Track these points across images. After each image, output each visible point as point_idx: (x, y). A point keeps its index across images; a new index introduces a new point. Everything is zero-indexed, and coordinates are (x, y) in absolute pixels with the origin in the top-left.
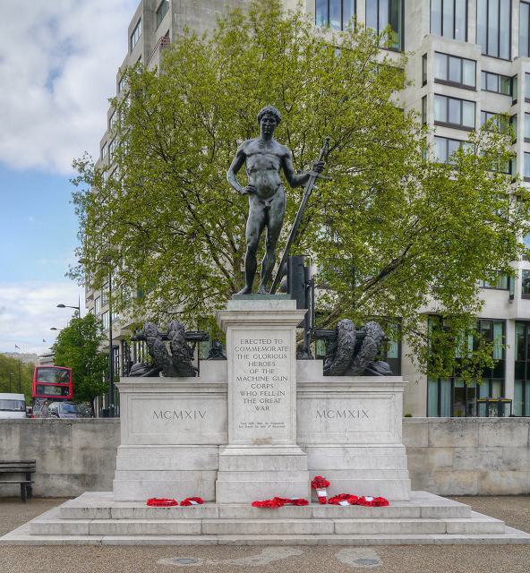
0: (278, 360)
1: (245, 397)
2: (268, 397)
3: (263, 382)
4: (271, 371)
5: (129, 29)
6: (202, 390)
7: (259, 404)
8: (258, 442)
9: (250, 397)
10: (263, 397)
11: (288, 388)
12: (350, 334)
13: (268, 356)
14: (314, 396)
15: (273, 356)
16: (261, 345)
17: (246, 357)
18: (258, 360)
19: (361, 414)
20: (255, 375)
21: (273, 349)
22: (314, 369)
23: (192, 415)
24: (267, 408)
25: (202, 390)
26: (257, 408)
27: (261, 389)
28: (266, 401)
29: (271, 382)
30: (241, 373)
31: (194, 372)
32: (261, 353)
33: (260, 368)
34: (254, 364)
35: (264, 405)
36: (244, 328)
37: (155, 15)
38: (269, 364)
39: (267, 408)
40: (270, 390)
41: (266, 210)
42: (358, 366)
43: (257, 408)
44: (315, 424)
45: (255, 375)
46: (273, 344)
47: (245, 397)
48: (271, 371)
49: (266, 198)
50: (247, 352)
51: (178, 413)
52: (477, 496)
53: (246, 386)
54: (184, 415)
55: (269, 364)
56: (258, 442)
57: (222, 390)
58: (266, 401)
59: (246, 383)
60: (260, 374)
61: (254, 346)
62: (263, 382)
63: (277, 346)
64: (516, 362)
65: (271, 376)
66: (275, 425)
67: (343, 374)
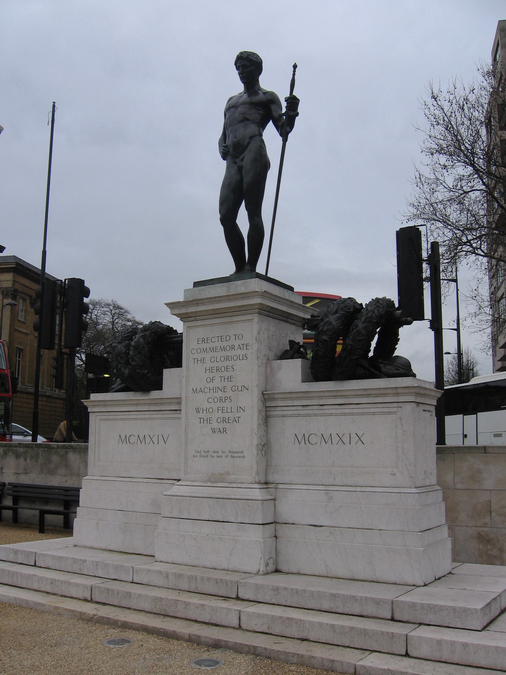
0: (238, 362)
1: (201, 415)
2: (226, 415)
3: (220, 394)
4: (230, 379)
7: (215, 425)
8: (215, 479)
10: (220, 414)
11: (251, 401)
13: (227, 358)
14: (290, 413)
15: (232, 358)
16: (219, 344)
17: (203, 360)
18: (215, 365)
20: (211, 385)
21: (233, 348)
22: (291, 373)
23: (155, 440)
24: (225, 430)
27: (219, 404)
28: (224, 420)
29: (229, 393)
33: (217, 375)
34: (211, 370)
35: (221, 426)
36: (200, 323)
38: (227, 369)
39: (225, 430)
40: (227, 404)
41: (240, 169)
43: (214, 432)
44: (290, 458)
45: (211, 385)
46: (232, 342)
47: (201, 415)
48: (230, 379)
49: (237, 157)
50: (203, 355)
52: (420, 624)
54: (148, 440)
56: (215, 479)
57: (176, 406)
58: (224, 420)
60: (217, 383)
62: (220, 394)
63: (237, 343)
64: (240, 78)
65: (229, 385)
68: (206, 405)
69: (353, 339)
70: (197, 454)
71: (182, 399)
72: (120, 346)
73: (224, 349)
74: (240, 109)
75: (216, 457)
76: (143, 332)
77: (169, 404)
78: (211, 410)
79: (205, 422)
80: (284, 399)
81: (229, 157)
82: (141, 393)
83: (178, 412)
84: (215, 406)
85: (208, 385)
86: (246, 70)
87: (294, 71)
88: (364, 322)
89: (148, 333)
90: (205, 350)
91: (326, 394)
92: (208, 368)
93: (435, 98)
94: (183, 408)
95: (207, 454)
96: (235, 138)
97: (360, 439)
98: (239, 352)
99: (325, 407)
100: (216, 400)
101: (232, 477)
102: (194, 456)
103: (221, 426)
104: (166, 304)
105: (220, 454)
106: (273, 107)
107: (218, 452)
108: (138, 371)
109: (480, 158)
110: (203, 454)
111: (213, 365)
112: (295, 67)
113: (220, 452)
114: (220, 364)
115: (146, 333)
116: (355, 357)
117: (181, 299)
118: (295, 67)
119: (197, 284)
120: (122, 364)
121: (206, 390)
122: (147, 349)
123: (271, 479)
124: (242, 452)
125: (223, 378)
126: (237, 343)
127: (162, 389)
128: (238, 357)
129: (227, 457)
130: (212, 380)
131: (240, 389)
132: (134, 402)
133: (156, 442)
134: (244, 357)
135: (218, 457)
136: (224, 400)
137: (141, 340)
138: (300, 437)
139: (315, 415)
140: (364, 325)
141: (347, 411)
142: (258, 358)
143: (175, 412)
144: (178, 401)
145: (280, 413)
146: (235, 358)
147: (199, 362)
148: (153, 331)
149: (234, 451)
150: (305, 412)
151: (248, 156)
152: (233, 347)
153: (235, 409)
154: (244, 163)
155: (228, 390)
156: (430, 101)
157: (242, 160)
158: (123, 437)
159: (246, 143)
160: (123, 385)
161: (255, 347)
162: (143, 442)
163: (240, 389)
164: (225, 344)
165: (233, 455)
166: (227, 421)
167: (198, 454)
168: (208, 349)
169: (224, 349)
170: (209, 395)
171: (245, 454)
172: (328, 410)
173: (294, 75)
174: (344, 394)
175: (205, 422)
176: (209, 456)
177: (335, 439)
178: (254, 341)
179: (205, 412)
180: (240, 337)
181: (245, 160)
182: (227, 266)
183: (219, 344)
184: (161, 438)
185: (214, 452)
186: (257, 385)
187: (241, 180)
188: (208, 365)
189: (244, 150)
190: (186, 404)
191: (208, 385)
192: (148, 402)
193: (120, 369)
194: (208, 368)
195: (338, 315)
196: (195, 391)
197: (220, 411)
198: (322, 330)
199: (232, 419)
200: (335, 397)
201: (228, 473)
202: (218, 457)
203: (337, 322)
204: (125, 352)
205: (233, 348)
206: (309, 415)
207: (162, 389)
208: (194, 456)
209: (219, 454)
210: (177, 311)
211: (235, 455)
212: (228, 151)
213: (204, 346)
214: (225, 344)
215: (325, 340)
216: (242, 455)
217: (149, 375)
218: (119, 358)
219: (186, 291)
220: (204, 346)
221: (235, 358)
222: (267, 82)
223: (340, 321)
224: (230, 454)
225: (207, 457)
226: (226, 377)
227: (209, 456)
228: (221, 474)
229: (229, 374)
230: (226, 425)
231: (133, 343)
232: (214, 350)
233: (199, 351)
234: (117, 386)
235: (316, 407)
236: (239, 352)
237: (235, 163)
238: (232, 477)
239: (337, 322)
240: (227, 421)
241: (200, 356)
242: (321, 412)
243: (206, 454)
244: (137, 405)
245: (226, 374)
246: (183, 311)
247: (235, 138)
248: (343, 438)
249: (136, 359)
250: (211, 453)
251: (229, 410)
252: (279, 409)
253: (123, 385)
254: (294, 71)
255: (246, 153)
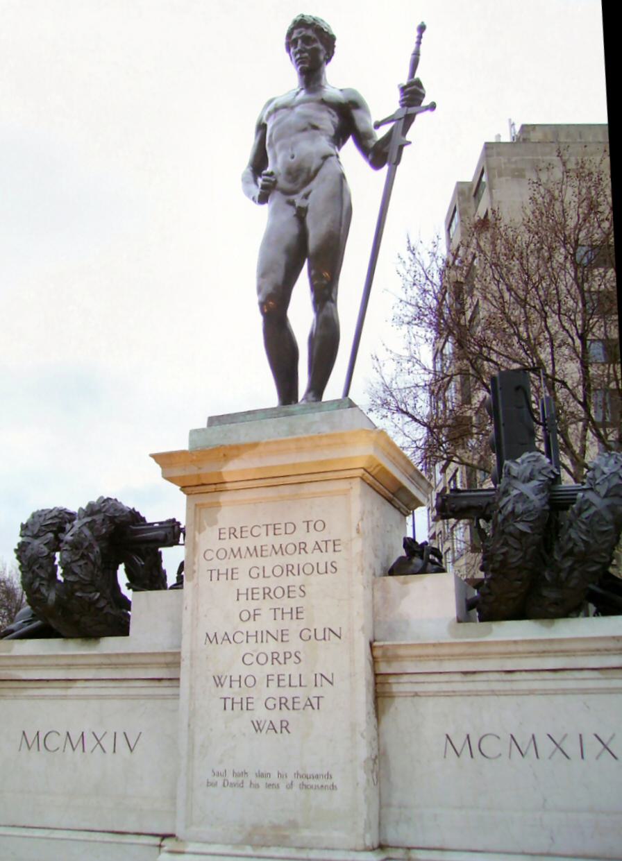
0: (315, 578)
1: (226, 691)
2: (288, 693)
3: (272, 646)
4: (297, 613)
5: (446, 221)
6: (128, 673)
7: (261, 713)
9: (235, 692)
12: (528, 489)
13: (288, 570)
14: (434, 688)
16: (268, 540)
17: (231, 574)
19: (572, 747)
20: (251, 627)
21: (302, 548)
23: (107, 743)
24: (285, 726)
25: (128, 673)
26: (258, 727)
27: (268, 669)
28: (283, 703)
29: (295, 644)
30: (216, 622)
31: (116, 622)
32: (269, 562)
33: (266, 606)
37: (472, 199)
38: (288, 592)
39: (285, 726)
40: (291, 668)
41: (301, 215)
42: (558, 584)
43: (258, 727)
45: (251, 627)
47: (226, 691)
48: (297, 613)
50: (233, 562)
51: (75, 738)
53: (227, 659)
54: (90, 742)
55: (288, 592)
57: (167, 671)
58: (283, 703)
59: (227, 649)
60: (266, 622)
61: (250, 542)
62: (272, 646)
63: (311, 538)
65: (294, 627)
66: (306, 780)
67: (519, 614)
68: (239, 670)
69: (588, 531)
70: (216, 779)
71: (183, 655)
72: (36, 542)
73: (282, 550)
74: (298, 110)
75: (262, 786)
76: (89, 516)
77: (144, 665)
78: (250, 681)
79: (237, 707)
80: (419, 658)
81: (276, 198)
82: (79, 641)
83: (175, 683)
84: (260, 672)
85: (244, 627)
86: (308, 48)
87: (420, 37)
88: (606, 496)
89: (99, 518)
90: (237, 553)
91: (521, 648)
92: (243, 591)
93: (412, 250)
94: (184, 675)
95: (240, 779)
96: (293, 157)
97: (606, 747)
98: (315, 557)
99: (478, 677)
100: (262, 659)
101: (306, 833)
102: (209, 784)
103: (276, 716)
104: (158, 457)
105: (274, 779)
106: (357, 114)
107: (268, 775)
108: (78, 594)
109: (534, 307)
110: (232, 779)
111: (254, 583)
112: (422, 29)
113: (275, 775)
114: (272, 583)
115: (95, 517)
116: (594, 569)
117: (184, 446)
118: (422, 29)
119: (213, 421)
120: (42, 579)
121: (239, 637)
122: (97, 549)
123: (392, 836)
124: (329, 776)
125: (279, 613)
126: (311, 538)
127: (127, 634)
128: (315, 568)
129: (290, 786)
130: (254, 615)
131: (320, 636)
132: (64, 661)
133: (109, 748)
134: (329, 567)
135: (268, 786)
136: (281, 659)
137: (87, 532)
138: (459, 742)
139: (493, 693)
140: (607, 501)
141: (571, 685)
142: (362, 571)
143: (157, 684)
144: (173, 660)
145: (408, 688)
146: (308, 569)
147: (223, 578)
148: (108, 514)
149: (309, 772)
150: (470, 686)
151: (319, 190)
152: (303, 546)
153: (308, 679)
154: (309, 202)
155: (293, 638)
156: (407, 255)
157: (306, 197)
158: (31, 736)
159: (313, 168)
160: (39, 622)
161: (357, 546)
162: (80, 747)
163: (320, 636)
164: (283, 540)
165: (306, 782)
166: (290, 704)
167: (220, 780)
168: (243, 550)
169: (282, 550)
170: (245, 648)
171: (336, 780)
172: (523, 682)
173: (419, 43)
174: (564, 647)
175: (237, 707)
176: (247, 784)
177: (545, 746)
178: (354, 534)
179: (236, 685)
180: (290, 528)
181: (311, 196)
182: (269, 396)
183: (268, 540)
184: (121, 741)
185: (260, 775)
186: (363, 629)
187: (303, 236)
188: (244, 583)
189: (310, 178)
190: (192, 665)
191: (244, 627)
192: (97, 660)
193: (38, 590)
194: (243, 591)
195: (535, 483)
196: (212, 639)
197: (273, 684)
198: (513, 512)
199: (303, 701)
200: (543, 654)
201: (294, 825)
202: (268, 786)
203: (539, 497)
204: (49, 554)
205: (302, 548)
206: (477, 694)
207: (127, 634)
208: (209, 784)
209: (270, 781)
210: (178, 472)
211: (312, 782)
212: (276, 182)
213: (235, 543)
214: (283, 540)
215: (523, 533)
216: (329, 783)
217: (102, 604)
218: (35, 568)
219: (194, 432)
220: (235, 543)
221: (308, 569)
222: (338, 77)
223: (543, 495)
224: (298, 782)
225: (241, 785)
226: (287, 610)
227: (247, 784)
228: (275, 827)
229: (293, 603)
230: (285, 714)
231: (68, 537)
232: (257, 552)
233: (222, 554)
234: (21, 626)
235: (497, 676)
236: (315, 557)
237: (292, 203)
238: (306, 833)
239: (539, 497)
240: (290, 704)
241: (223, 566)
242: (508, 686)
243: (239, 779)
244: (69, 666)
245: (288, 604)
246: (192, 470)
247: (293, 157)
248: (565, 746)
249: (77, 570)
250: (252, 777)
251: (295, 682)
252: (405, 678)
253: (39, 622)
254: (420, 37)
255: (314, 184)
